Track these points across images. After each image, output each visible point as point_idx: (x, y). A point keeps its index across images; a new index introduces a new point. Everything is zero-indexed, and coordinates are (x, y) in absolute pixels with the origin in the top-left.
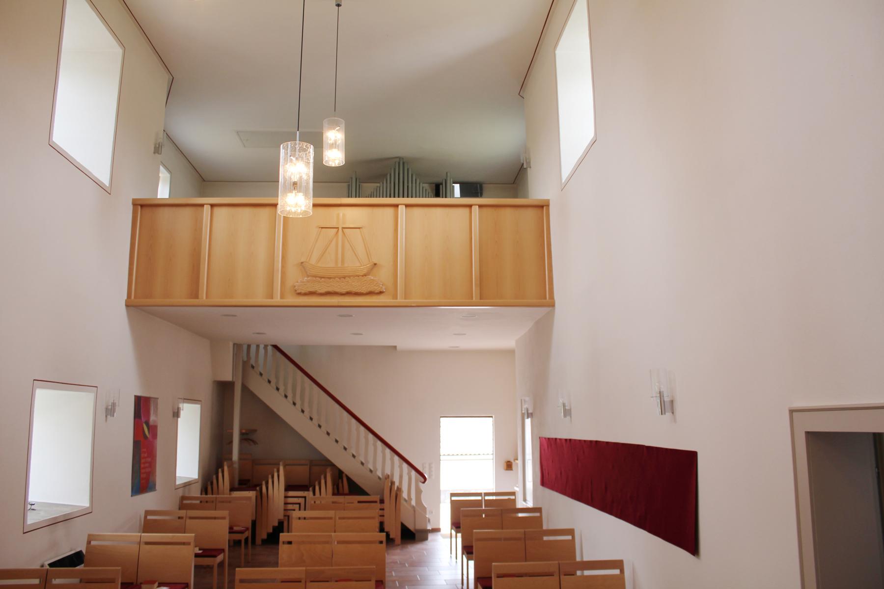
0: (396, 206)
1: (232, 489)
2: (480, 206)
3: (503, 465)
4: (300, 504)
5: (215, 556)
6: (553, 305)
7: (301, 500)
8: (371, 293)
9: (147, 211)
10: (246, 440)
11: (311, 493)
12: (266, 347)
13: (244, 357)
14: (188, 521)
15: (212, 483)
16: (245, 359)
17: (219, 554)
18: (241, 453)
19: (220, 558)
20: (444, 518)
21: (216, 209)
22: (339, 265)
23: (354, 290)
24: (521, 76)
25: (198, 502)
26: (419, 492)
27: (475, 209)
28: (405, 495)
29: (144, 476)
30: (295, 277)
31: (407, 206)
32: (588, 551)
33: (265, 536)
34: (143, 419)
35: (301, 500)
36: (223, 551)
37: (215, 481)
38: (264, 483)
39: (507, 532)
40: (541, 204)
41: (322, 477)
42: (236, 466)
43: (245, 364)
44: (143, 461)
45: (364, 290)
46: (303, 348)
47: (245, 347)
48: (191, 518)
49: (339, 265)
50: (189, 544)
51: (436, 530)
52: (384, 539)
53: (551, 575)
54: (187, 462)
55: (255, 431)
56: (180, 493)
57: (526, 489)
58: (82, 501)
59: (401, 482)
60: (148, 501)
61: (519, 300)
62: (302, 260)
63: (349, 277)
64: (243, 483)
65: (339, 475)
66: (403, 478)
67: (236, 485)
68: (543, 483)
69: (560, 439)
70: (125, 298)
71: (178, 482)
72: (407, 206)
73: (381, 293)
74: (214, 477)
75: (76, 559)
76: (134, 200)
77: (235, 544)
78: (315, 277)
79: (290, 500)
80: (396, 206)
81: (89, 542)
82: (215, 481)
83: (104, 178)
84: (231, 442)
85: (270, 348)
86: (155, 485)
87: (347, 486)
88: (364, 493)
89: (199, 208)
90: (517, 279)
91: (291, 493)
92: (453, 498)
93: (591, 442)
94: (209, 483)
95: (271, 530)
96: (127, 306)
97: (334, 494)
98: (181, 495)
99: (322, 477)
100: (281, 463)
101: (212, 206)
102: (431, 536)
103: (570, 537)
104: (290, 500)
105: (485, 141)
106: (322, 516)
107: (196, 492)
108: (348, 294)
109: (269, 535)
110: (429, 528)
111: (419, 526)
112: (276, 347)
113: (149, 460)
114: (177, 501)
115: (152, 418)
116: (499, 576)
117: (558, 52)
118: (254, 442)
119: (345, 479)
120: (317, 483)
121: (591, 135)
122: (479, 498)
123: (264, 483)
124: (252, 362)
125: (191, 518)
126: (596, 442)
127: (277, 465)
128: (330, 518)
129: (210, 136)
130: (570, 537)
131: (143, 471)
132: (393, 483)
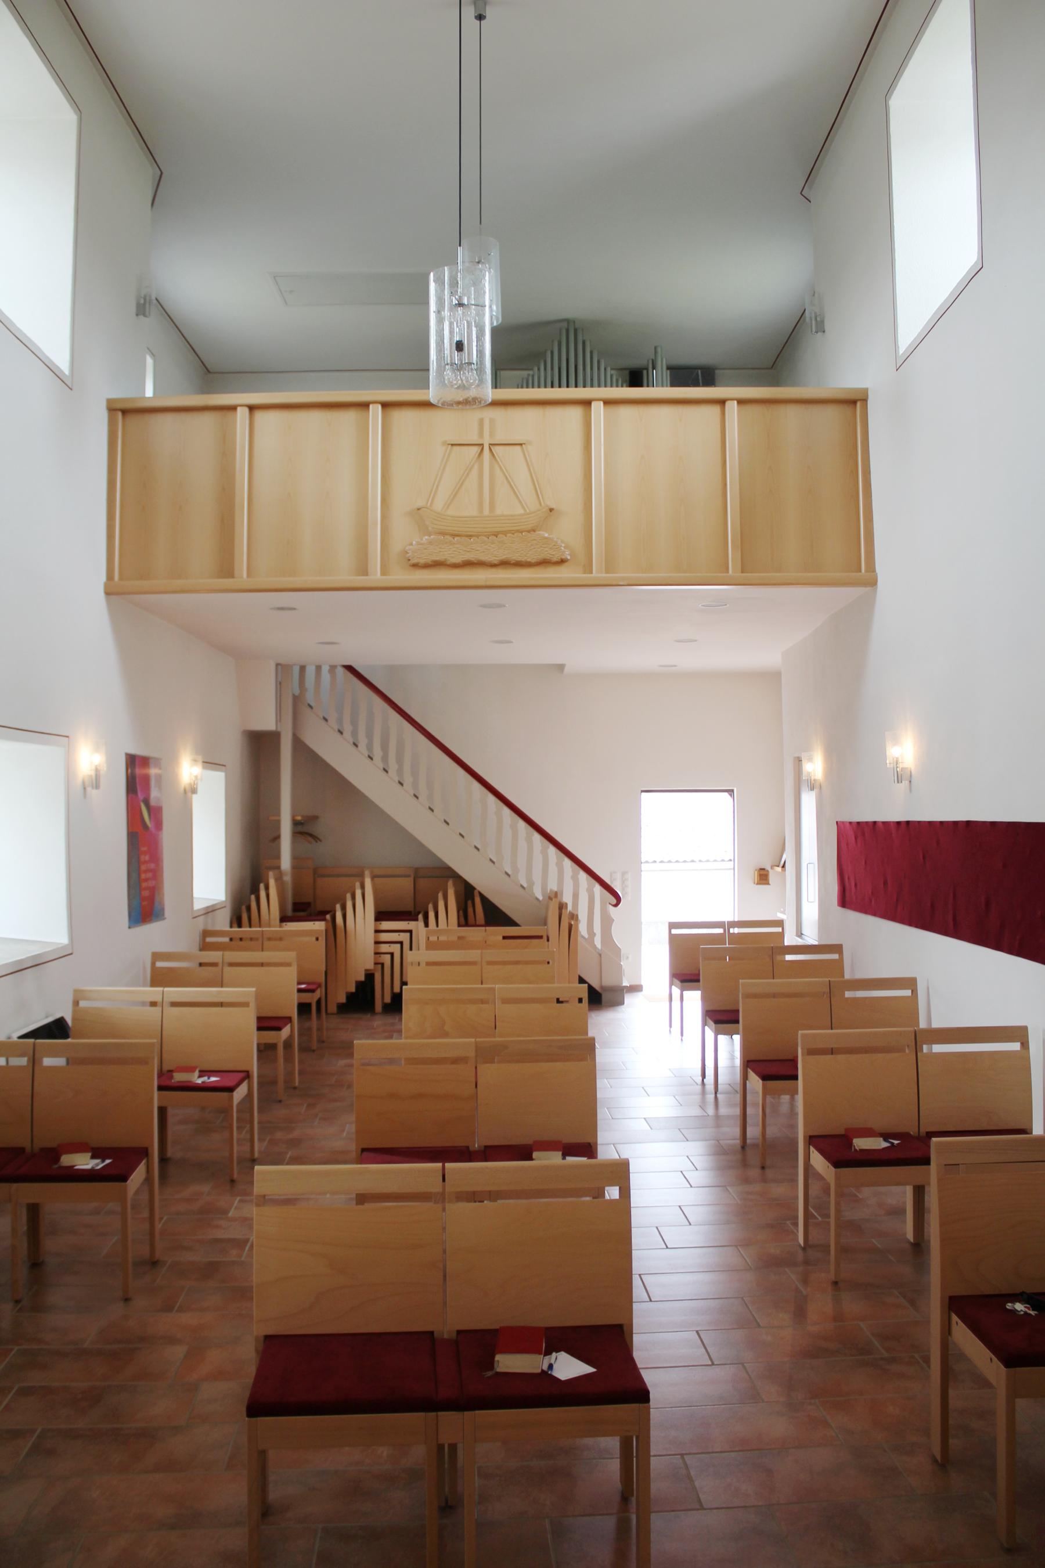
0: (587, 403)
1: (284, 919)
2: (741, 402)
3: (752, 875)
4: (401, 943)
5: (279, 1029)
6: (873, 583)
7: (404, 937)
8: (544, 563)
9: (134, 420)
10: (301, 833)
11: (421, 923)
12: (333, 668)
13: (293, 683)
14: (227, 969)
15: (249, 909)
16: (297, 692)
17: (286, 1025)
18: (295, 858)
19: (286, 1032)
20: (650, 964)
21: (259, 415)
22: (486, 512)
23: (515, 557)
24: (816, 149)
25: (226, 940)
26: (607, 922)
27: (732, 407)
28: (583, 928)
29: (146, 893)
30: (405, 536)
31: (607, 402)
32: (940, 1012)
33: (342, 999)
34: (141, 796)
35: (404, 937)
36: (289, 1019)
37: (254, 905)
38: (338, 907)
39: (778, 983)
40: (853, 397)
41: (440, 895)
42: (288, 878)
43: (297, 700)
44: (143, 867)
45: (532, 558)
46: (393, 670)
47: (296, 670)
48: (231, 965)
49: (486, 512)
50: (246, 1005)
51: (636, 989)
52: (585, 996)
53: (900, 1050)
54: (207, 871)
55: (315, 818)
56: (201, 924)
57: (806, 908)
58: (58, 935)
59: (575, 904)
60: (154, 936)
61: (812, 572)
62: (420, 503)
63: (505, 533)
64: (301, 909)
65: (467, 892)
66: (581, 897)
67: (289, 912)
68: (844, 902)
69: (885, 824)
70: (103, 578)
71: (198, 906)
72: (607, 402)
73: (562, 561)
74: (253, 897)
75: (57, 1029)
76: (109, 401)
77: (304, 1009)
78: (443, 534)
79: (384, 937)
80: (587, 403)
81: (76, 1003)
82: (254, 905)
83: (62, 361)
84: (277, 838)
85: (340, 671)
86: (163, 909)
87: (480, 910)
88: (510, 922)
89: (229, 414)
90: (806, 530)
91: (386, 925)
92: (674, 931)
93: (955, 824)
94: (244, 908)
95: (352, 989)
96: (107, 593)
97: (459, 925)
98: (201, 927)
99: (440, 895)
100: (367, 873)
101: (252, 408)
102: (629, 999)
103: (907, 993)
104: (384, 937)
105: (728, 280)
106: (457, 959)
107: (222, 921)
108: (504, 564)
109: (350, 996)
110: (625, 983)
111: (608, 981)
112: (350, 669)
113: (152, 866)
114: (197, 938)
115: (154, 793)
116: (811, 1052)
117: (897, 102)
118: (315, 838)
119: (478, 900)
120: (431, 906)
121: (971, 257)
122: (720, 931)
123: (338, 907)
124: (310, 697)
125: (231, 965)
126: (968, 823)
127: (361, 876)
128: (474, 963)
129: (223, 285)
130: (907, 993)
131: (144, 885)
132: (562, 906)
